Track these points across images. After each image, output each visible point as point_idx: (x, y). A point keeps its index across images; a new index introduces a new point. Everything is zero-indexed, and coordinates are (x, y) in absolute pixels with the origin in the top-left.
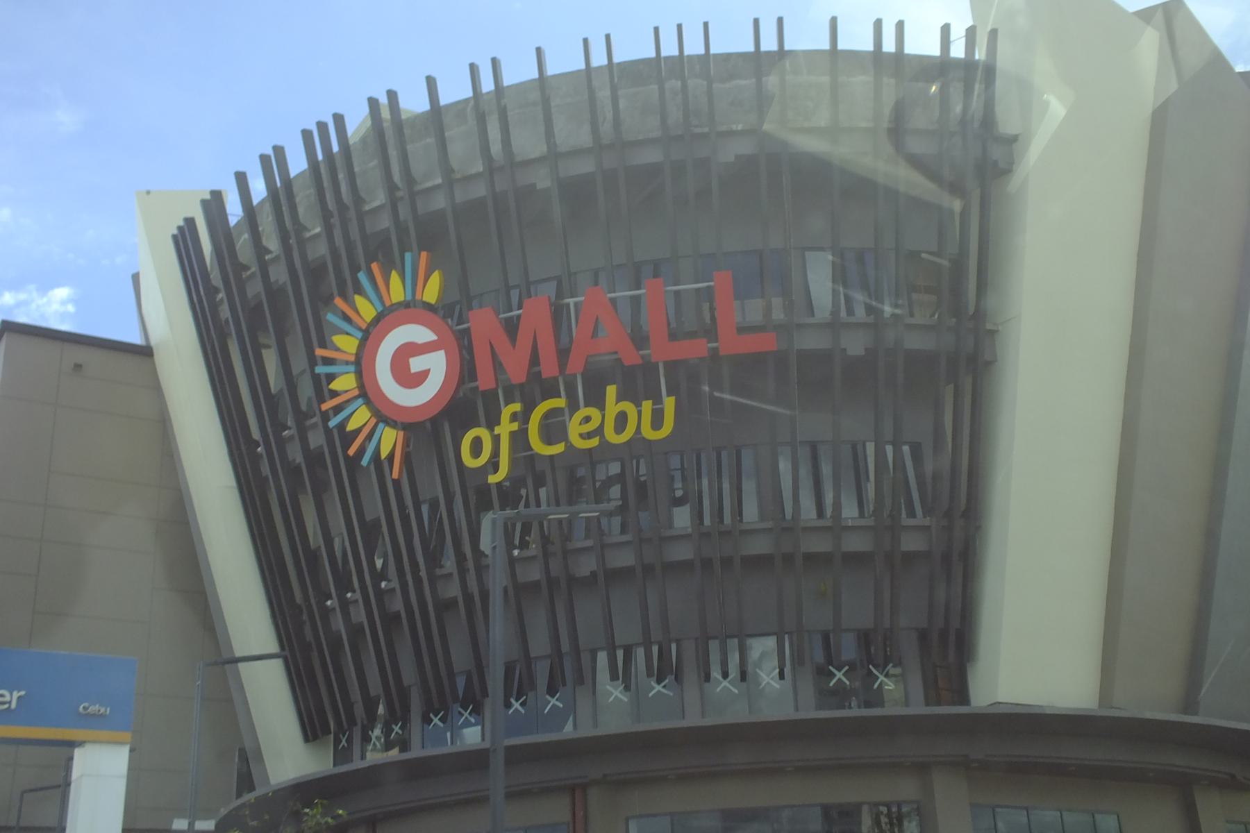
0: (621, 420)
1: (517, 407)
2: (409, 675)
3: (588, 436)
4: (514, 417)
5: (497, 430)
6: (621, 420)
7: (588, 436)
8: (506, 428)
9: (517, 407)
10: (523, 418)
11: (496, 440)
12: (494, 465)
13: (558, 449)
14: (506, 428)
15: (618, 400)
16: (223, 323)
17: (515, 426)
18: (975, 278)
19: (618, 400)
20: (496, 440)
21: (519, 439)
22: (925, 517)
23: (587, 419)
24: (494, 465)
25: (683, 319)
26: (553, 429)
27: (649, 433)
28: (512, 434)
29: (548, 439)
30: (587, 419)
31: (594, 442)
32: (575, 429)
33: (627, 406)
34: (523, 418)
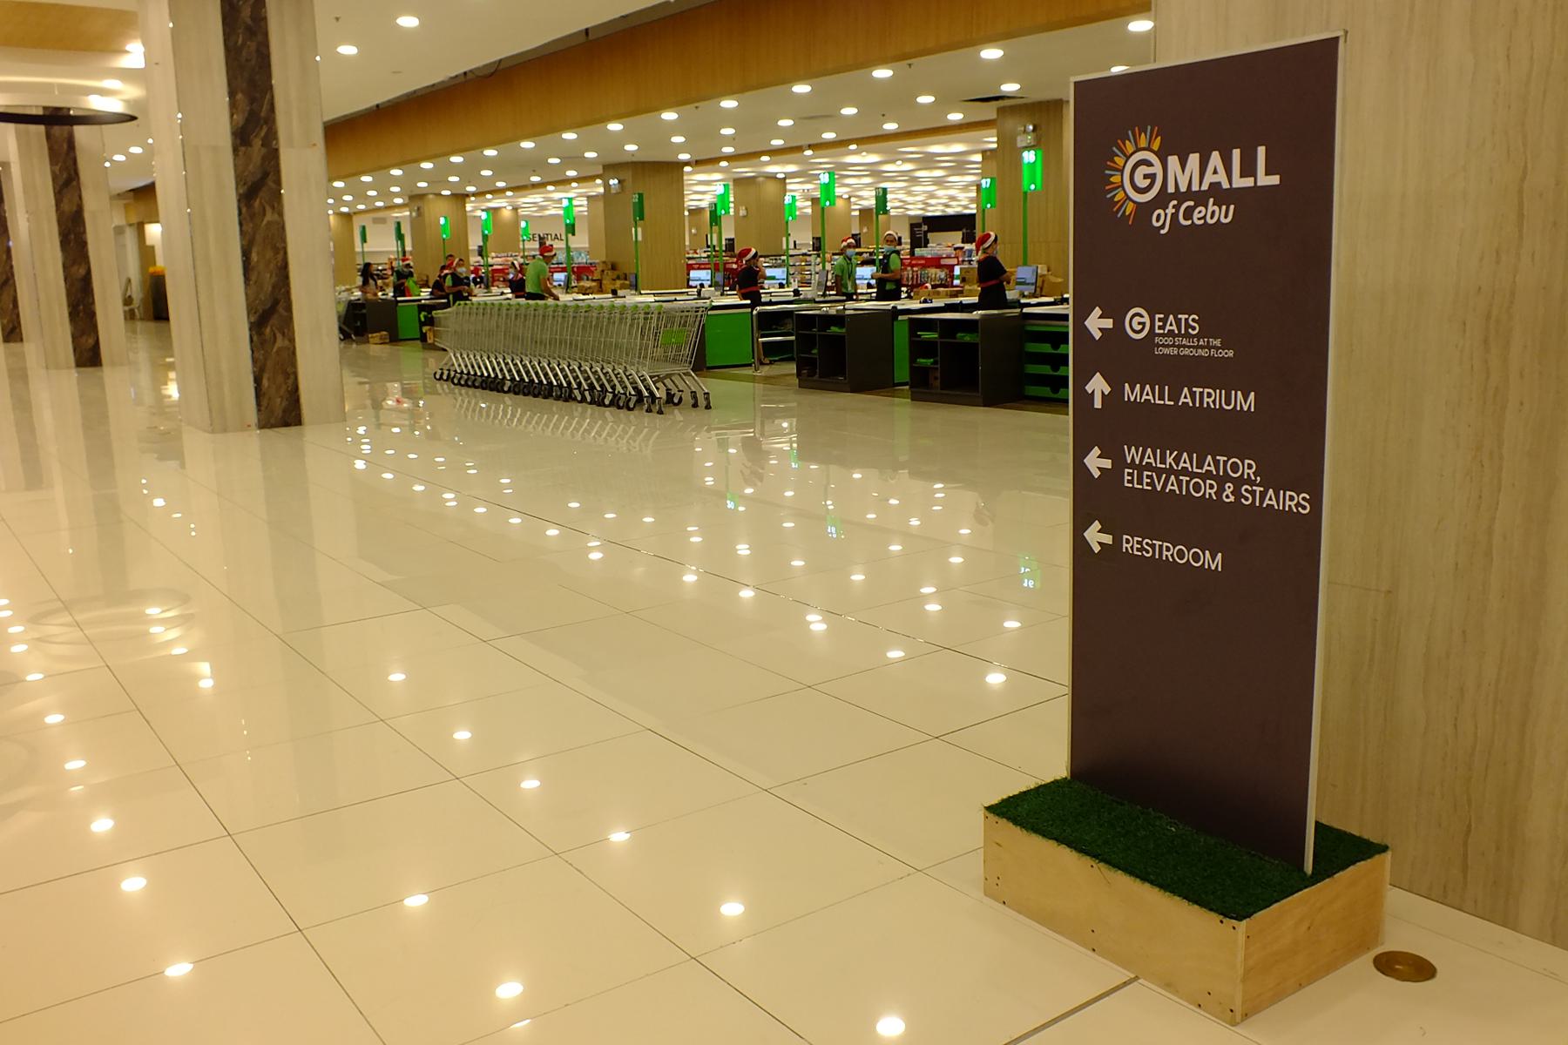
0: (1213, 213)
1: (1175, 202)
2: (599, 333)
3: (1199, 219)
4: (1174, 207)
5: (1167, 211)
6: (1213, 213)
7: (1199, 219)
8: (1170, 211)
9: (1175, 202)
10: (1177, 207)
11: (1166, 215)
12: (1163, 227)
13: (1189, 222)
14: (1170, 211)
15: (1214, 204)
16: (60, 164)
17: (1174, 211)
18: (1316, 773)
19: (1214, 204)
20: (1166, 215)
21: (1175, 216)
22: (674, 394)
23: (1200, 212)
24: (1163, 227)
25: (153, 163)
26: (1189, 214)
27: (1224, 221)
28: (1172, 214)
29: (1185, 219)
30: (1200, 212)
31: (1202, 222)
32: (1196, 215)
33: (1216, 208)
34: (1177, 207)
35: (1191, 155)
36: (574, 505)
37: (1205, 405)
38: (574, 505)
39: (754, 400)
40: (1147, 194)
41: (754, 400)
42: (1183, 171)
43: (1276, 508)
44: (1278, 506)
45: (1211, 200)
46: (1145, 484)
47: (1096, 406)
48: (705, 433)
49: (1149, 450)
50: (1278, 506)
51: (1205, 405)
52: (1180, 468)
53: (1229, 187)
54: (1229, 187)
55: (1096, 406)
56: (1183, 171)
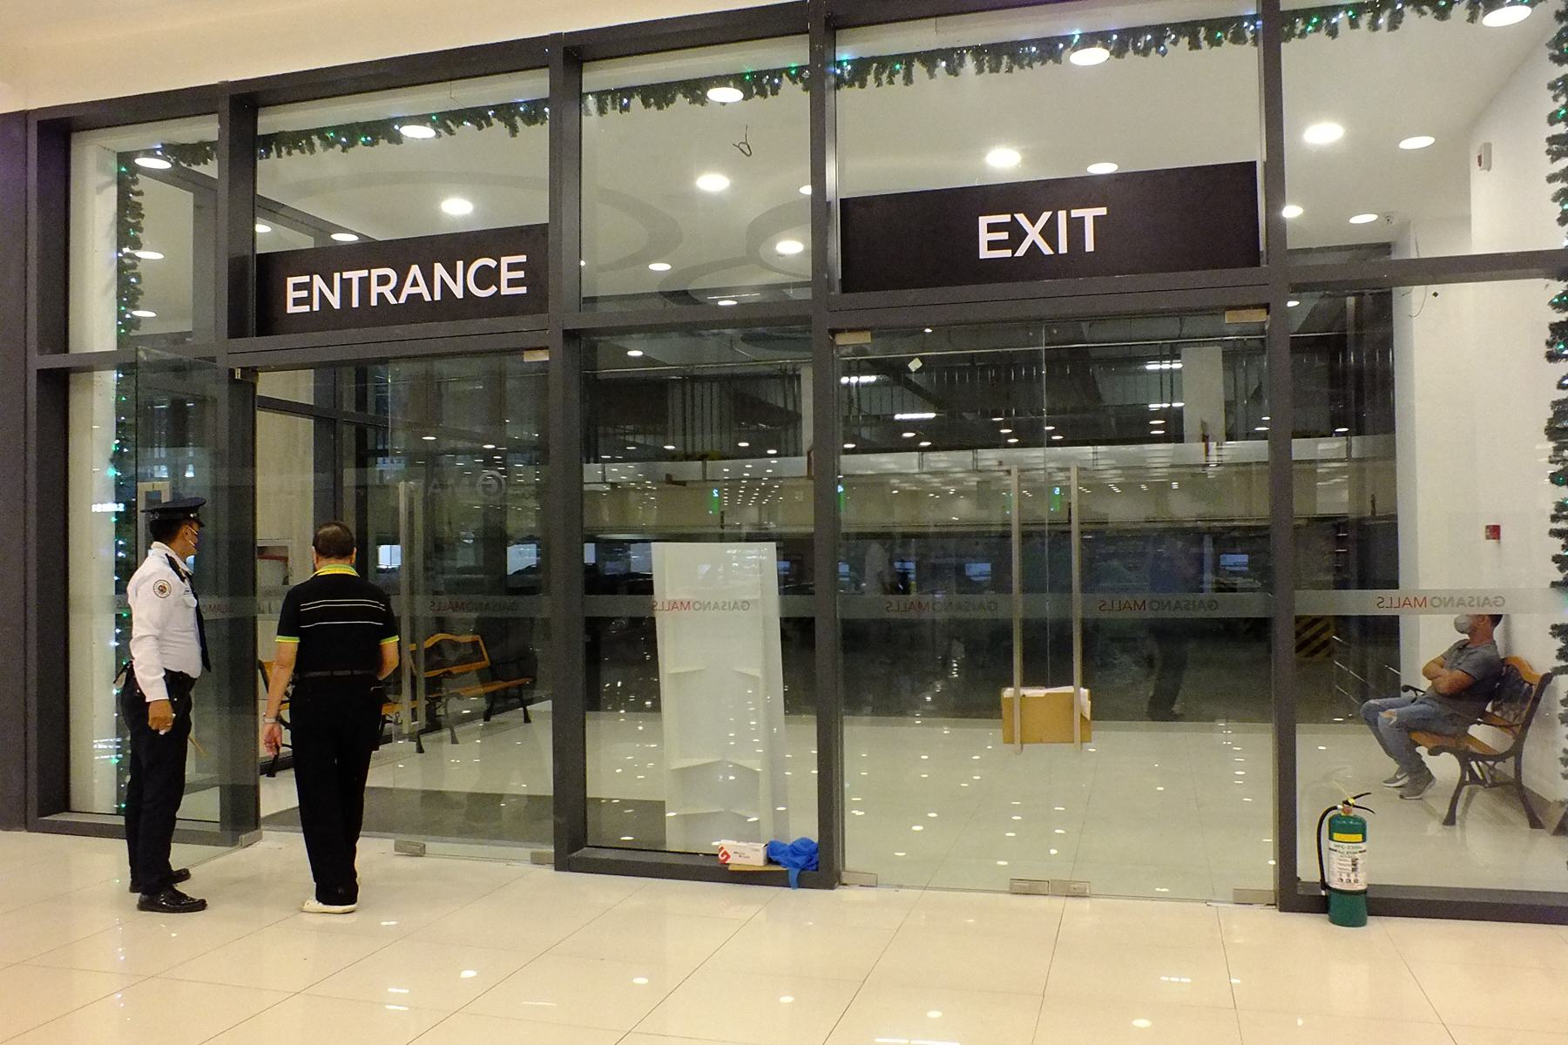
35: (403, 302)
36: (468, 974)
37: (374, 302)
38: (468, 974)
39: (685, 435)
40: (481, 264)
41: (685, 435)
42: (320, 289)
43: (427, 298)
44: (432, 293)
45: (1103, 211)
46: (504, 283)
47: (1105, 213)
48: (880, 569)
49: (336, 305)
50: (432, 293)
51: (374, 302)
52: (402, 300)
53: (430, 299)
54: (430, 299)
55: (1105, 213)
56: (320, 289)
